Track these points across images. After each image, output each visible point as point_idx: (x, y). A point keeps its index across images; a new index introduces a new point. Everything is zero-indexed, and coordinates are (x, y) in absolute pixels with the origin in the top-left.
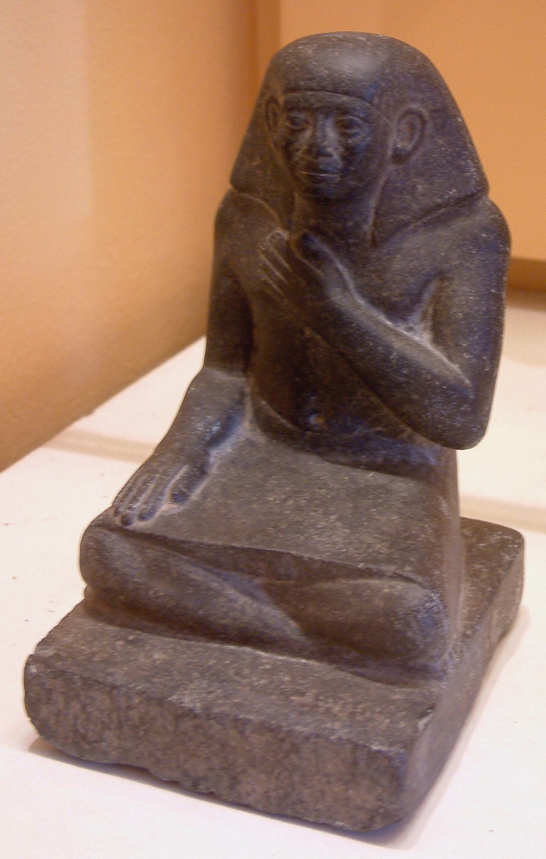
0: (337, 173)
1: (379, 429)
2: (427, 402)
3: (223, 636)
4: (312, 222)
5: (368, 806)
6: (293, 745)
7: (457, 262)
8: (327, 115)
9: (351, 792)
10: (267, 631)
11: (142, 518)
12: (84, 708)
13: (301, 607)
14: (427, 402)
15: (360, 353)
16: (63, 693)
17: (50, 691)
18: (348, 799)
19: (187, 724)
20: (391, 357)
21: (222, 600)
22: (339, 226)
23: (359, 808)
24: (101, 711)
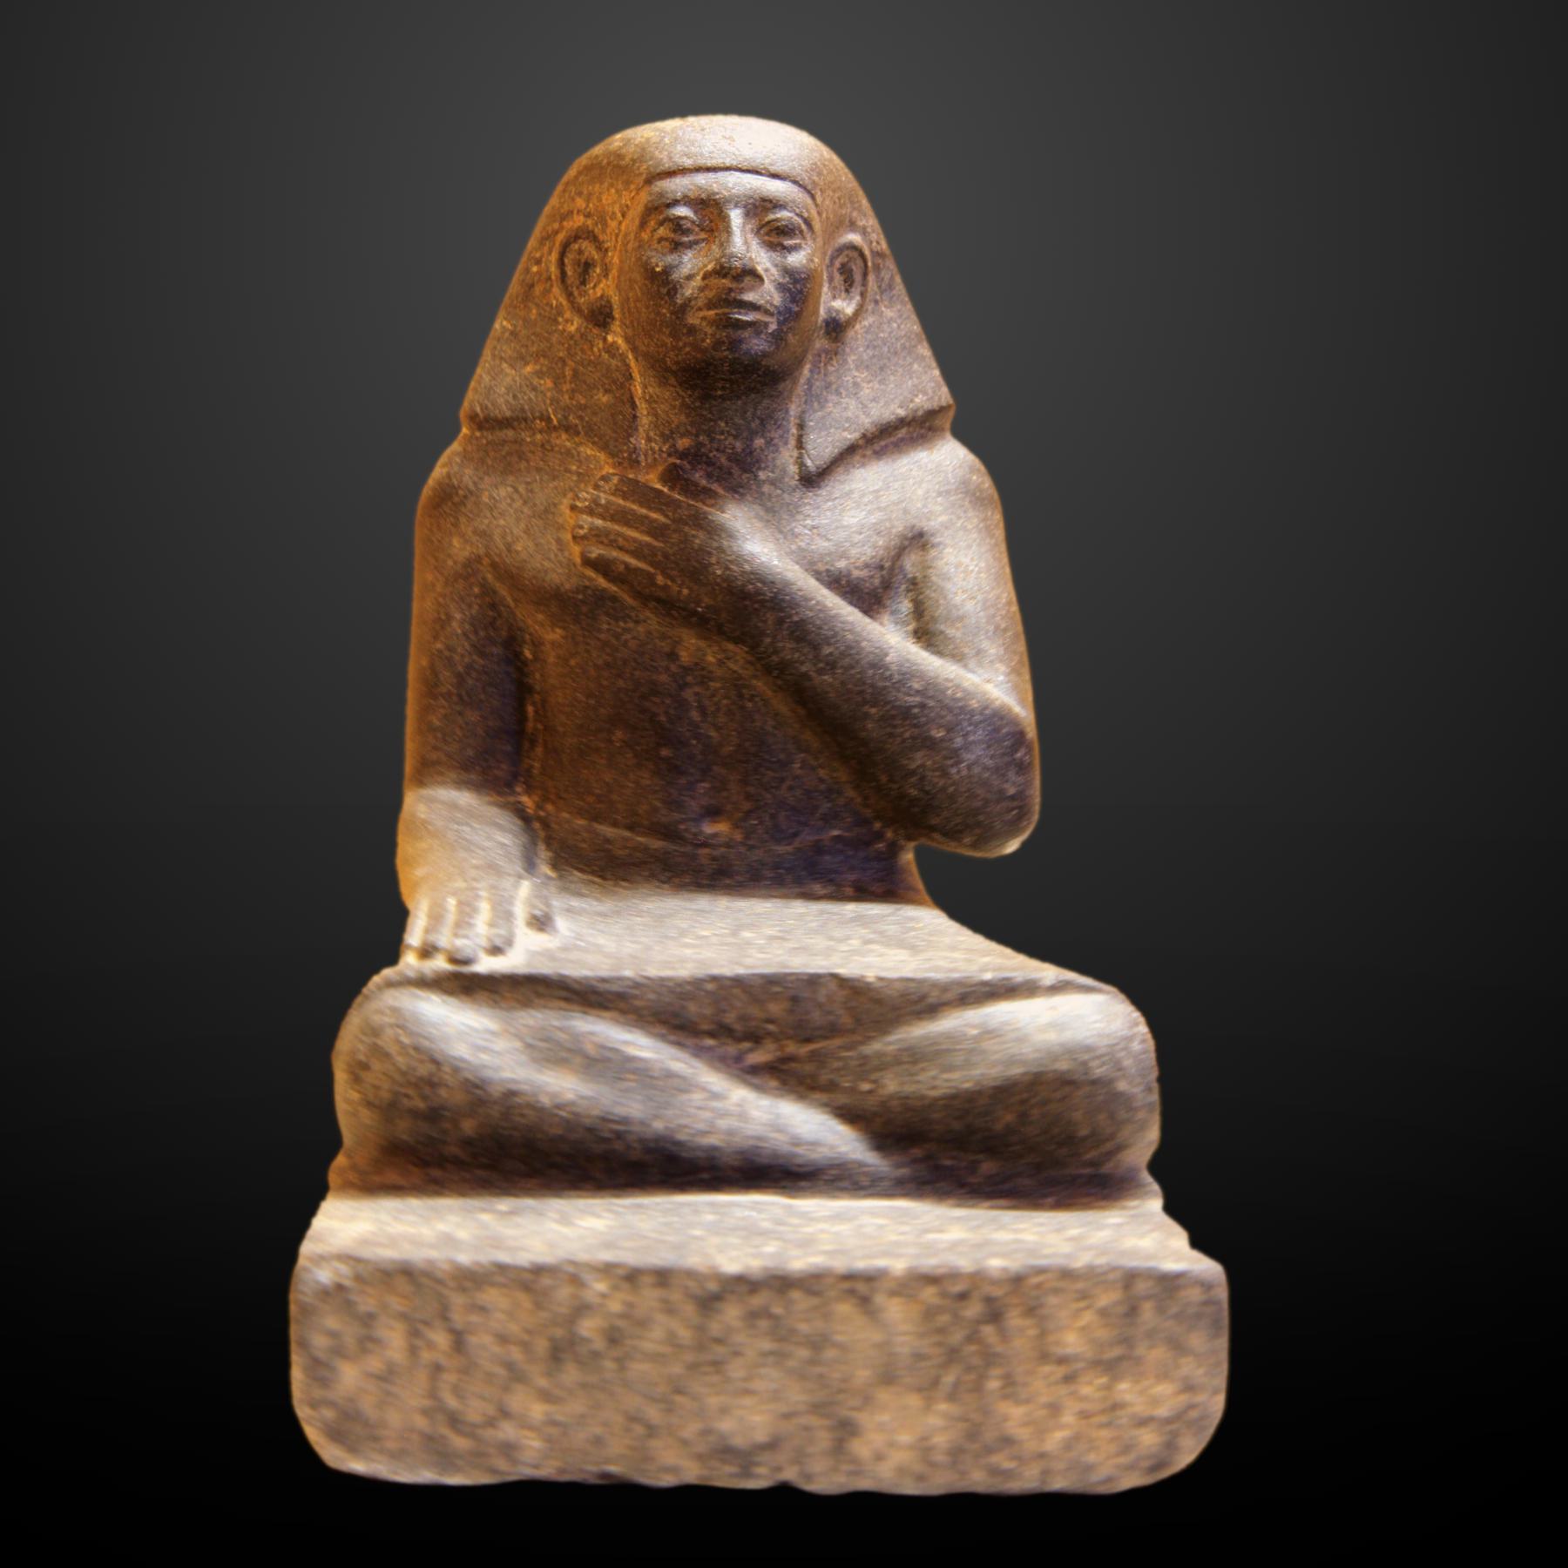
0: (772, 315)
1: (836, 833)
2: (959, 741)
3: (705, 1176)
4: (683, 443)
5: (1163, 1411)
6: (989, 1300)
7: (943, 518)
8: (736, 206)
9: (1123, 1386)
10: (799, 1150)
11: (496, 950)
12: (459, 1341)
13: (866, 1087)
14: (959, 741)
15: (827, 655)
16: (403, 1317)
17: (368, 1320)
18: (1116, 1407)
19: (732, 1313)
20: (888, 659)
21: (697, 1097)
22: (739, 445)
23: (1143, 1422)
24: (503, 1339)
